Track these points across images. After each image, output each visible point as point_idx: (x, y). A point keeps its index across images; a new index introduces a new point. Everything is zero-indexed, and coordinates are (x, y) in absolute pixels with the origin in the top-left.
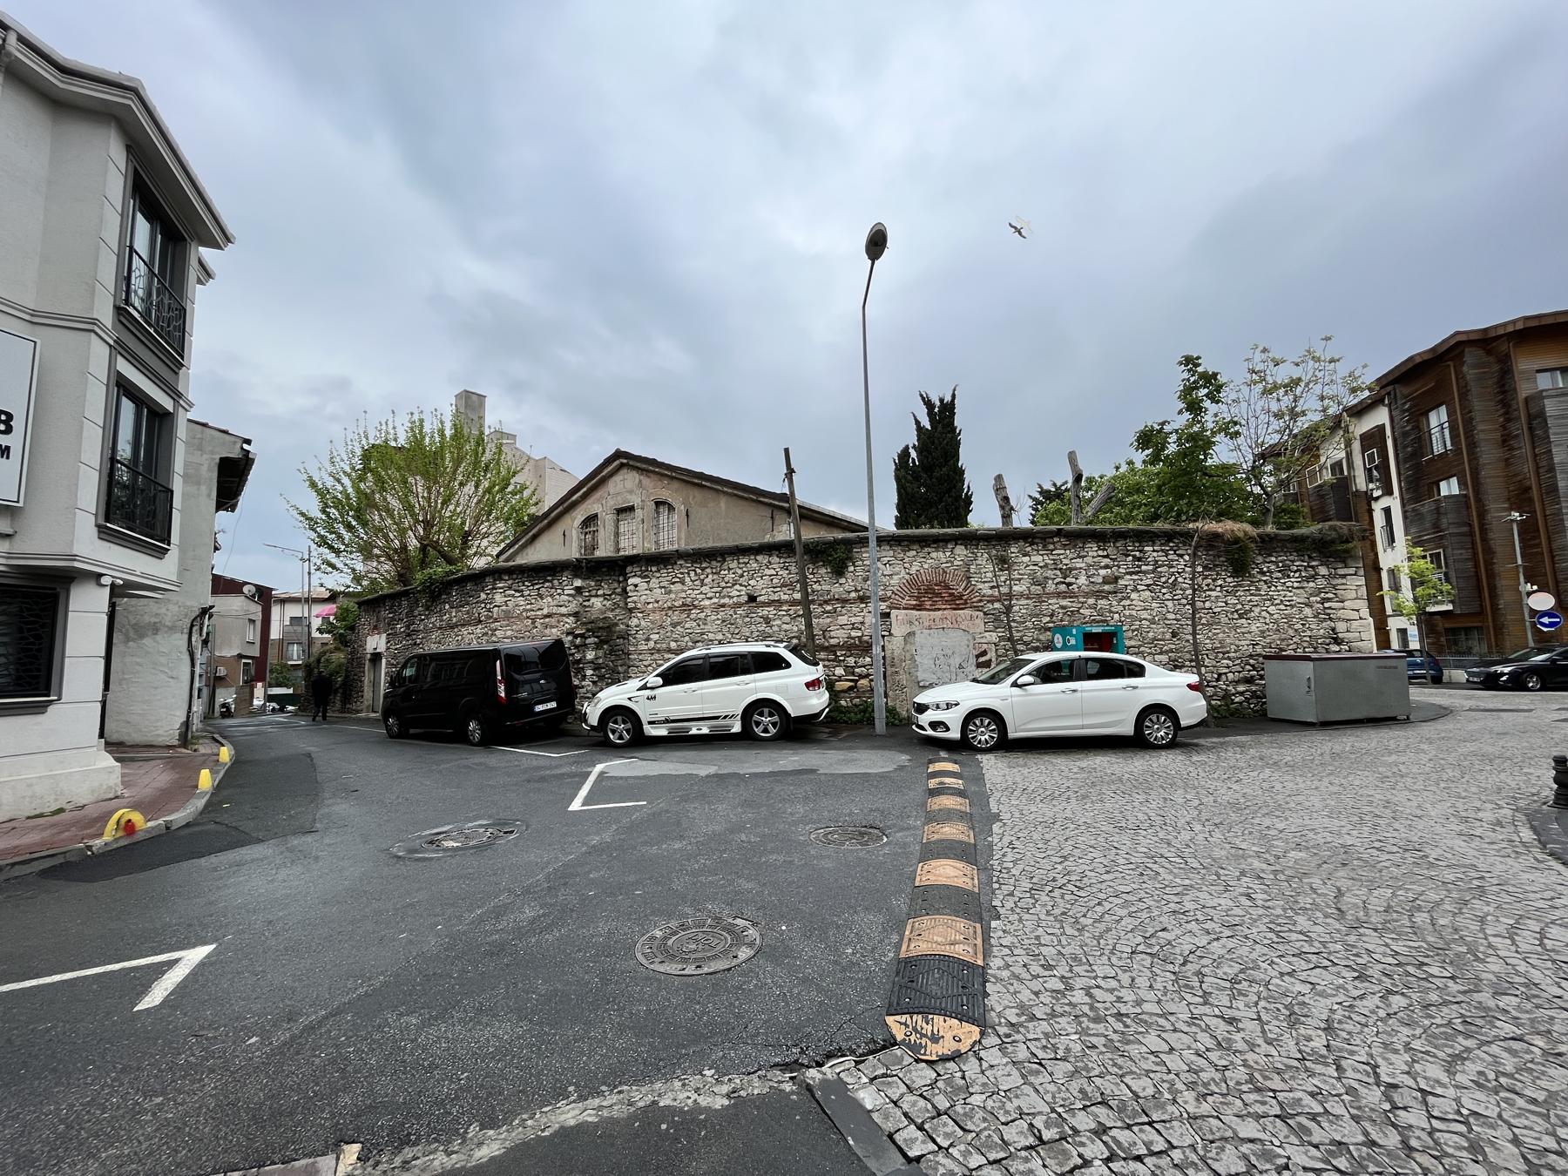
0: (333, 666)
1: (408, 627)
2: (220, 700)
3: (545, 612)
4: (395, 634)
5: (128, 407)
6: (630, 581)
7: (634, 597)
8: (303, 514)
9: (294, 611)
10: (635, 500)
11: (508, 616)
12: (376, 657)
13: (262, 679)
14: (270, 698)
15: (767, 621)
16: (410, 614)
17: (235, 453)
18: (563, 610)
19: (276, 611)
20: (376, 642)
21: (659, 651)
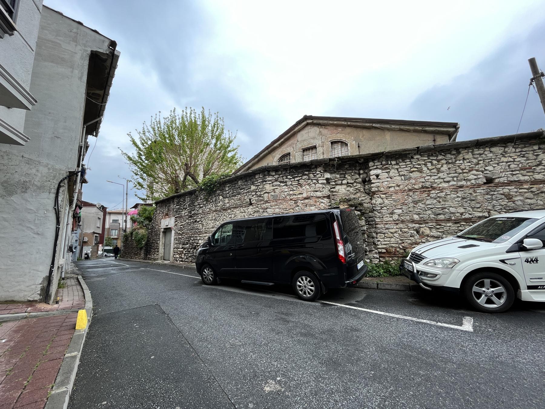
0: (140, 236)
1: (190, 212)
2: (84, 252)
3: (305, 195)
4: (181, 217)
6: (372, 172)
7: (375, 185)
8: (129, 157)
9: (113, 217)
10: (317, 142)
11: (276, 199)
12: (167, 230)
14: (105, 251)
15: (509, 197)
16: (192, 204)
17: (104, 49)
18: (319, 194)
19: (107, 217)
20: (168, 222)
21: (403, 222)
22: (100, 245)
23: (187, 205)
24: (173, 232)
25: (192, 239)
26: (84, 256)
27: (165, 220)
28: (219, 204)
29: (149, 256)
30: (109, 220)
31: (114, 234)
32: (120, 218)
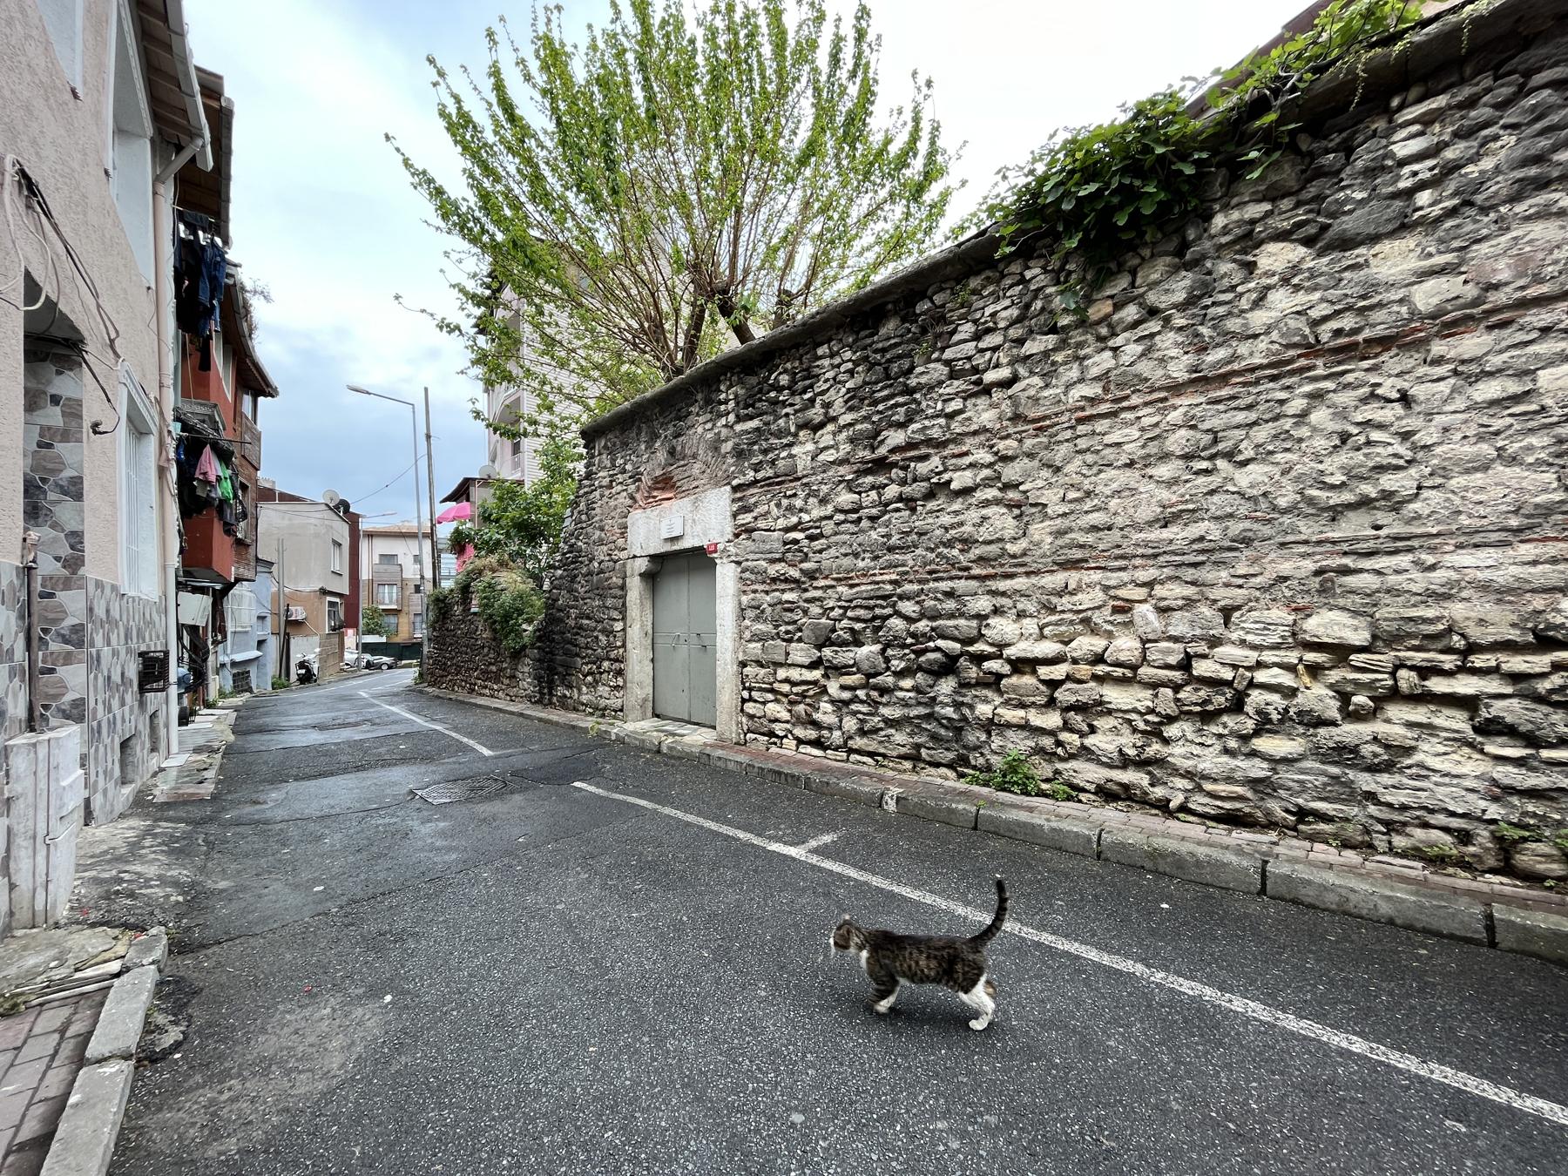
0: (506, 598)
5: (1262, 820)
9: (383, 547)
12: (681, 565)
13: (355, 625)
19: (364, 545)
22: (350, 632)
23: (837, 398)
24: (726, 574)
25: (908, 607)
26: (295, 672)
27: (653, 513)
28: (1259, 319)
29: (560, 691)
30: (370, 555)
31: (388, 598)
32: (404, 551)
